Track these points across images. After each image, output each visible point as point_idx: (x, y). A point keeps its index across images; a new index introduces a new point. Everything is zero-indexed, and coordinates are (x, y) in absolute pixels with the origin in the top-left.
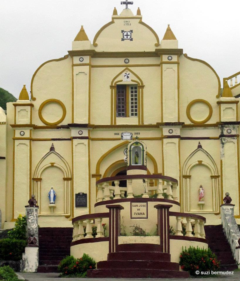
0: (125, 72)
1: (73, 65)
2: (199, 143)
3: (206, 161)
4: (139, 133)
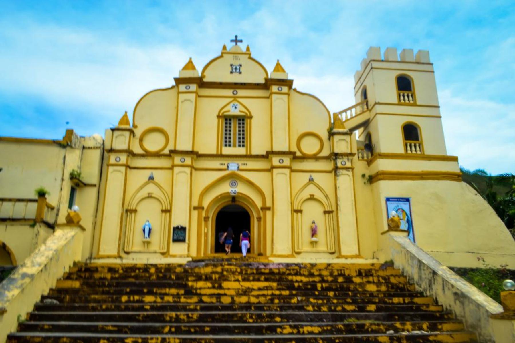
1: (179, 93)
2: (311, 176)
3: (319, 195)
4: (247, 164)
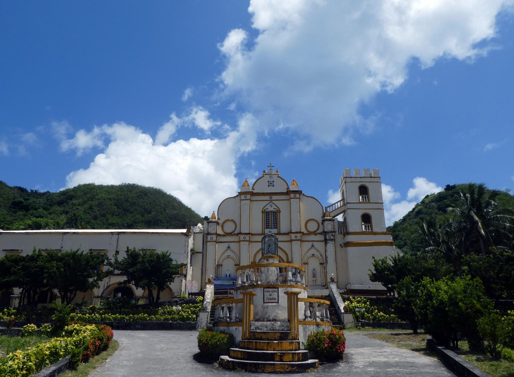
0: (270, 204)
1: (241, 200)
3: (317, 254)
